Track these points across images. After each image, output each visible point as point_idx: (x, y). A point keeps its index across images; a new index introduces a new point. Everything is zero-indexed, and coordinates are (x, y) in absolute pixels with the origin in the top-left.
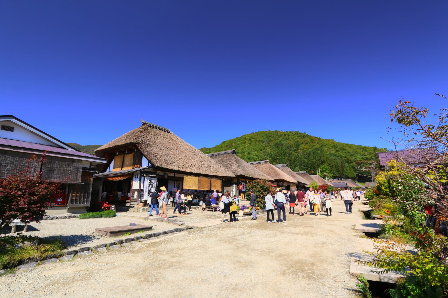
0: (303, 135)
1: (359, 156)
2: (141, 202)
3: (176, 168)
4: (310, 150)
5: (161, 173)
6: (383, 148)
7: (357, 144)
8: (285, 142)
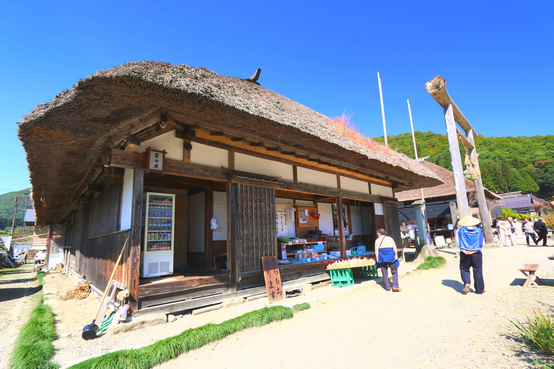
0: (426, 135)
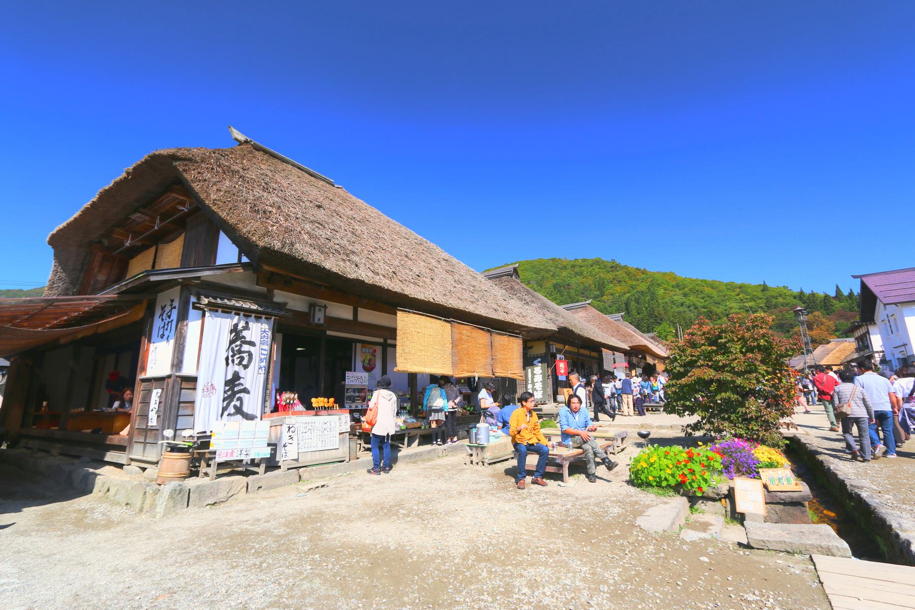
1: (735, 305)
2: (174, 449)
3: (364, 275)
4: (628, 295)
5: (296, 302)
6: (781, 285)
7: (726, 280)
8: (574, 281)
